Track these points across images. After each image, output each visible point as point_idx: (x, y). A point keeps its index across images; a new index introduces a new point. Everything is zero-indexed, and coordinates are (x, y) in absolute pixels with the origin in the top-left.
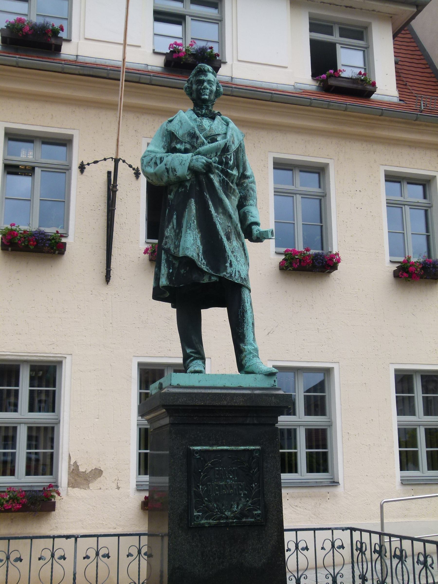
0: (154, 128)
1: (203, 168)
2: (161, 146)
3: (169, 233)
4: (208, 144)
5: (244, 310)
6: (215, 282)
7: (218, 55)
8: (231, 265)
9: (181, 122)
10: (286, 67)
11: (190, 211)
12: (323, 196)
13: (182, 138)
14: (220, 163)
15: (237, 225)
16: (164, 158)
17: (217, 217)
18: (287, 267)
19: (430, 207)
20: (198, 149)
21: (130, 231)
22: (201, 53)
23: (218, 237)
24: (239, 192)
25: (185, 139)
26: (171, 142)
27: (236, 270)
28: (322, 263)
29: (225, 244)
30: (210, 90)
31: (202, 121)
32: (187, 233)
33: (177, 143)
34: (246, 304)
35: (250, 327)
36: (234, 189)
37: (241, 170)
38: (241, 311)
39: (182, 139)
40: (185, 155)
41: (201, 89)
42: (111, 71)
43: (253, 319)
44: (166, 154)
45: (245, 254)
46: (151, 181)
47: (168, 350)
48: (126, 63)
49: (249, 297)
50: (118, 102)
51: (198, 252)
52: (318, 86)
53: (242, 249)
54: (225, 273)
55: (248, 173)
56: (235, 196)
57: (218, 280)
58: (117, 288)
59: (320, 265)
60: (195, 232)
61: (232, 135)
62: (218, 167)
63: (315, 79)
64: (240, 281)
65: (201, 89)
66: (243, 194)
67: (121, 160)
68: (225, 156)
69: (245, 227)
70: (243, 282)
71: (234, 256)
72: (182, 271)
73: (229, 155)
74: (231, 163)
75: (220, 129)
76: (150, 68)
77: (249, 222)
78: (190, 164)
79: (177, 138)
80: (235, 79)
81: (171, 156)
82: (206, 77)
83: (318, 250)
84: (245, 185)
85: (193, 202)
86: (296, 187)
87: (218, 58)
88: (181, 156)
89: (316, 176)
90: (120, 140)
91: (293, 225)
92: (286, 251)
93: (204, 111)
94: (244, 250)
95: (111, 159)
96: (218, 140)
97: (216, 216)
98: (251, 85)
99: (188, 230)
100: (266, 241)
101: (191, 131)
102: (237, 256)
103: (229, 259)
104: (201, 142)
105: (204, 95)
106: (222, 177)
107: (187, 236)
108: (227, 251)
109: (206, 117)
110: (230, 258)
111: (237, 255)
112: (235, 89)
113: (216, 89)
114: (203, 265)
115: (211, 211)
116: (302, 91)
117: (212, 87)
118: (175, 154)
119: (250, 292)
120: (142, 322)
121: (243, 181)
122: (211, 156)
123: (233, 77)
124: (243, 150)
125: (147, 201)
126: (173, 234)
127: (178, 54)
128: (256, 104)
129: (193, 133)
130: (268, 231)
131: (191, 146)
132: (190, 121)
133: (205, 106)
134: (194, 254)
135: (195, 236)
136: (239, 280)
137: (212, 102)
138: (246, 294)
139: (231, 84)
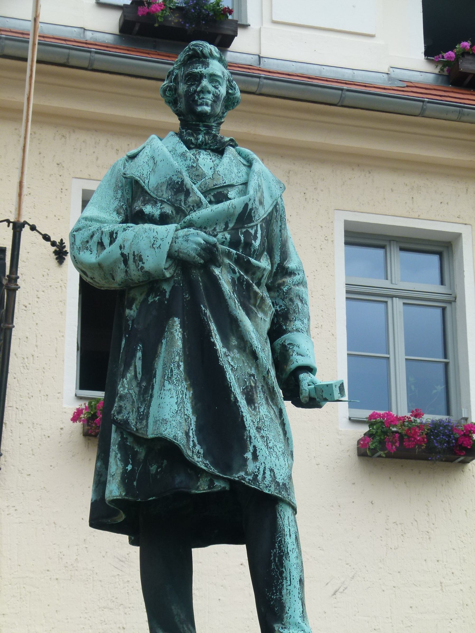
0: (97, 159)
1: (199, 255)
2: (111, 209)
3: (126, 389)
4: (208, 204)
5: (282, 551)
6: (223, 492)
7: (231, 12)
8: (255, 457)
9: (154, 159)
10: (372, 36)
11: (171, 343)
12: (450, 302)
13: (155, 192)
14: (234, 243)
15: (268, 372)
16: (119, 233)
17: (227, 356)
18: (374, 451)
19: (450, 302)
20: (189, 214)
21: (44, 372)
22: (194, 8)
23: (230, 397)
24: (273, 303)
25: (162, 195)
26: (134, 199)
27: (265, 468)
28: (448, 442)
29: (242, 412)
30: (213, 95)
31: (198, 157)
32: (164, 390)
33: (145, 203)
34: (288, 539)
35: (295, 587)
36: (262, 299)
37: (277, 259)
38: (275, 553)
39: (157, 195)
40: (161, 229)
41: (195, 91)
42: (7, 42)
43: (302, 571)
44: (121, 225)
45: (285, 433)
46: (91, 281)
47: (119, 628)
48: (40, 25)
49: (293, 523)
50: (23, 104)
51: (186, 428)
52: (439, 75)
53: (277, 422)
54: (242, 474)
55: (292, 265)
56: (265, 313)
57: (227, 488)
58: (12, 494)
59: (444, 447)
60: (180, 388)
61: (259, 186)
62: (229, 252)
63: (433, 60)
64: (275, 490)
65: (195, 91)
66: (281, 306)
67: (26, 226)
68: (244, 230)
69: (284, 376)
70: (280, 491)
71: (263, 437)
72: (153, 469)
73: (252, 227)
74: (257, 244)
75: (233, 175)
76: (89, 35)
77: (293, 366)
78: (171, 246)
79: (146, 192)
80: (266, 60)
81: (132, 228)
82: (205, 68)
83: (440, 415)
84: (285, 289)
85: (177, 326)
86: (392, 283)
87: (230, 17)
88: (154, 229)
89: (435, 259)
90: (25, 184)
91: (384, 361)
92: (372, 417)
93: (201, 137)
94: (283, 424)
95: (6, 223)
96: (229, 196)
97: (225, 353)
98: (299, 72)
99: (166, 383)
100: (328, 406)
101: (175, 178)
102: (268, 438)
103: (251, 443)
104: (195, 202)
105: (202, 104)
106: (238, 274)
107: (163, 394)
108: (247, 426)
109: (205, 149)
110: (253, 440)
111: (268, 435)
112: (265, 81)
113: (227, 92)
114: (197, 455)
115: (214, 344)
116: (405, 84)
117: (217, 88)
118: (141, 226)
119: (296, 513)
120: (66, 567)
121: (280, 281)
122: (215, 229)
123: (261, 55)
124: (281, 216)
125: (80, 310)
126: (134, 391)
127: (148, 8)
128: (308, 111)
129: (178, 182)
130: (332, 384)
131: (175, 210)
132: (172, 158)
133: (205, 126)
134: (179, 432)
135: (181, 396)
136: (272, 488)
137: (219, 119)
138: (286, 518)
139: (258, 70)
